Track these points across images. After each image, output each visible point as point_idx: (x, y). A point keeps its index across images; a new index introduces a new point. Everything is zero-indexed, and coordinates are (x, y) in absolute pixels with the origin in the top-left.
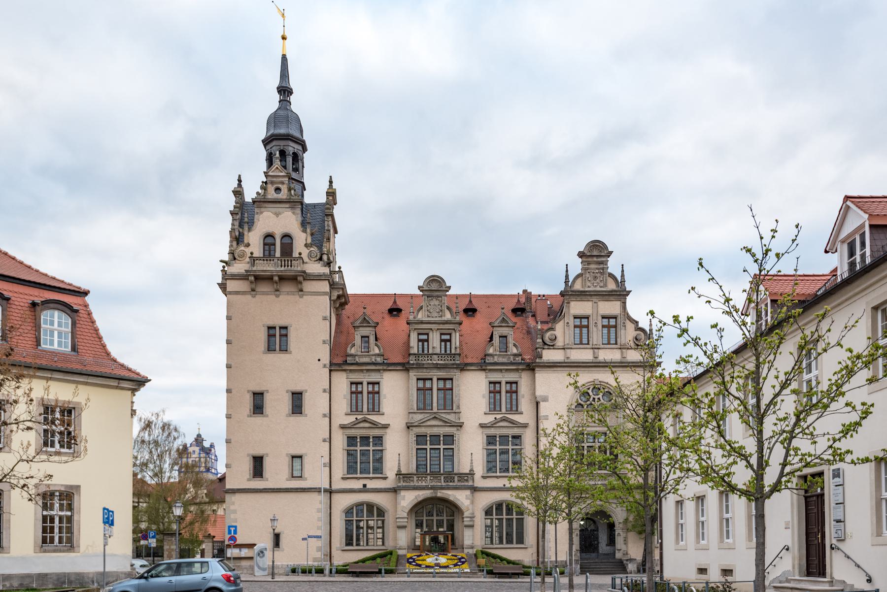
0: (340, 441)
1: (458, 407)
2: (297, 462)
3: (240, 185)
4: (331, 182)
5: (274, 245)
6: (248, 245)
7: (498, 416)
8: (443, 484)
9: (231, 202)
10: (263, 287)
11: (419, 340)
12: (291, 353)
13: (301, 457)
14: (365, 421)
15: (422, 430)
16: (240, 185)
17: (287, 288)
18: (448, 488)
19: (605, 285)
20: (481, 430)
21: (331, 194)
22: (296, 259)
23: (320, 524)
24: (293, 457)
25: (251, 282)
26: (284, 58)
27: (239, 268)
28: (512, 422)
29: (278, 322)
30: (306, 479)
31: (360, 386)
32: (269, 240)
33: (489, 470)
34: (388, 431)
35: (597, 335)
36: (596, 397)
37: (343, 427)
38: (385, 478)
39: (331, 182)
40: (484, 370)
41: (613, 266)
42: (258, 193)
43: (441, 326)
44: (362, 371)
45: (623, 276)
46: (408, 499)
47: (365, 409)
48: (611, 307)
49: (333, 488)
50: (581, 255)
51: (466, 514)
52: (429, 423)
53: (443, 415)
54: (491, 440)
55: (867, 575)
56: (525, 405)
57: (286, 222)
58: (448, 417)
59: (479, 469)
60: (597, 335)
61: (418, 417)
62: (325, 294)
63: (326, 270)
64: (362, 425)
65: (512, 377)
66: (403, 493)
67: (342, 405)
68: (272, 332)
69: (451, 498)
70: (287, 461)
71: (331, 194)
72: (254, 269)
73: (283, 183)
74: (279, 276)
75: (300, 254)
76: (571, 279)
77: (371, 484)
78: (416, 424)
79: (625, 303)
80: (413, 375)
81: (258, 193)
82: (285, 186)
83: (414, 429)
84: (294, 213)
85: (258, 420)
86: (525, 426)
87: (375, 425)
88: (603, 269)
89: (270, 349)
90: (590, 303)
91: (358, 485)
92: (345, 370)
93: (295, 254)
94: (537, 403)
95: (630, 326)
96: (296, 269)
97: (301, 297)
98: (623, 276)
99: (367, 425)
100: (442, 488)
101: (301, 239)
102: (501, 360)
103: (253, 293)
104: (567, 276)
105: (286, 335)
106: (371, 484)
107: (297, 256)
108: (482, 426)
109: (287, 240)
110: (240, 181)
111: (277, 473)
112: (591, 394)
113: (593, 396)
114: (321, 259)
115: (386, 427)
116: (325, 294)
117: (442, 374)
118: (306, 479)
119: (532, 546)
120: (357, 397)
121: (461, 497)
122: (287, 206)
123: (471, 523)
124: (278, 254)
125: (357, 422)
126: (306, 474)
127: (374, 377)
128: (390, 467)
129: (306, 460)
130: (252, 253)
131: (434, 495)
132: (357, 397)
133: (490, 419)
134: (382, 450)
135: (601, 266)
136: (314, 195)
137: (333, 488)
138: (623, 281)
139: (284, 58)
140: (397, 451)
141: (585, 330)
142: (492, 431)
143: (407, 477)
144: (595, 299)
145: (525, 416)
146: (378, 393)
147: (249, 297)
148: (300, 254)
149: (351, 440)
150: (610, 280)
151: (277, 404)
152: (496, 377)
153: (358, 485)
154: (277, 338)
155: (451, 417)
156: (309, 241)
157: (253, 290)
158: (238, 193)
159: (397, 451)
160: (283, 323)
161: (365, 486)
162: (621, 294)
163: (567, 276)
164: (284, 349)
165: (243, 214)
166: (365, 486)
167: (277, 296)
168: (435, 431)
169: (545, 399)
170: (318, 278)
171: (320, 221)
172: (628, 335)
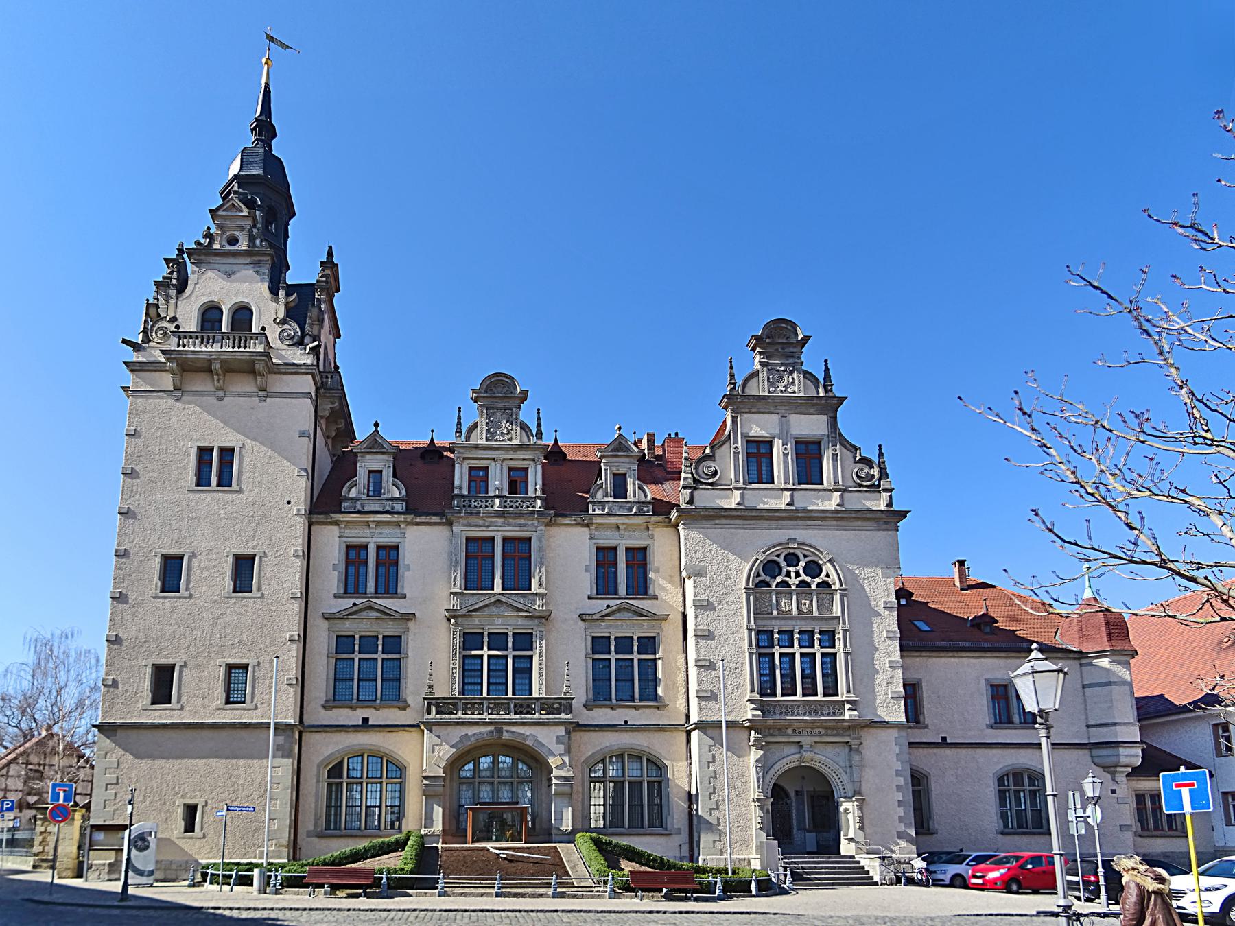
10: (201, 384)
14: (370, 608)
17: (245, 384)
21: (329, 265)
22: (255, 337)
23: (901, 781)
33: (595, 698)
34: (411, 624)
36: (792, 569)
37: (328, 617)
40: (587, 526)
42: (198, 243)
44: (367, 523)
47: (371, 587)
49: (307, 722)
57: (249, 288)
59: (580, 696)
64: (363, 615)
67: (330, 580)
71: (329, 265)
73: (242, 228)
74: (223, 362)
75: (264, 329)
77: (375, 717)
82: (246, 233)
84: (257, 272)
85: (170, 601)
88: (793, 365)
89: (202, 480)
90: (775, 418)
91: (355, 716)
92: (337, 523)
96: (252, 349)
97: (263, 399)
99: (375, 614)
103: (178, 393)
106: (375, 717)
111: (200, 700)
115: (408, 617)
116: (309, 395)
119: (679, 832)
120: (357, 572)
122: (248, 260)
132: (357, 572)
135: (791, 361)
136: (303, 269)
142: (602, 630)
143: (442, 705)
144: (782, 410)
147: (170, 402)
149: (343, 644)
151: (209, 576)
153: (355, 716)
154: (215, 467)
156: (281, 314)
159: (433, 661)
161: (365, 720)
166: (365, 720)
167: (220, 398)
168: (497, 626)
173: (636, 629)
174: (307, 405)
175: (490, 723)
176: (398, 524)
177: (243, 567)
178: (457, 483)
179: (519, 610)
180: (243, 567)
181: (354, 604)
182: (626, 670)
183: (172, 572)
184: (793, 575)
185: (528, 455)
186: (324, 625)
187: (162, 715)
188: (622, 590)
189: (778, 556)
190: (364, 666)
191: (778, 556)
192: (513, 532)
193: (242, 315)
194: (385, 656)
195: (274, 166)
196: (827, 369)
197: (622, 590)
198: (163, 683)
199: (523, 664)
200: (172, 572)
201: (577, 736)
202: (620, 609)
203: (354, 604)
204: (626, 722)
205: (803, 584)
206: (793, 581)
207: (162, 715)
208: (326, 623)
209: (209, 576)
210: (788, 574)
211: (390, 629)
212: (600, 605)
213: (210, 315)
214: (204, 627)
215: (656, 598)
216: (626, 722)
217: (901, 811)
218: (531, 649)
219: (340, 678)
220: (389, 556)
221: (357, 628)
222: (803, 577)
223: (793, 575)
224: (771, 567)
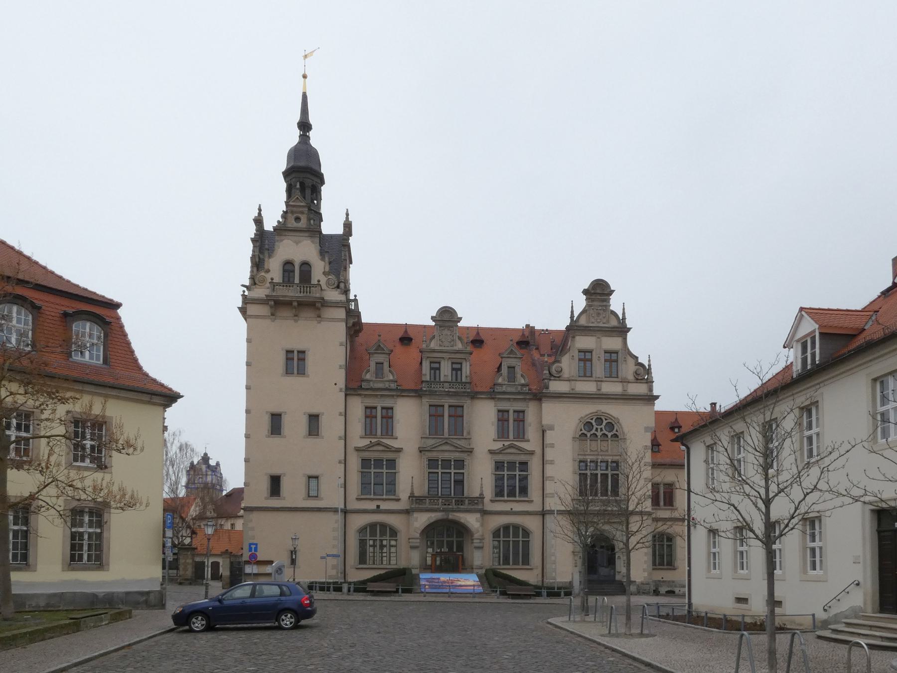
0: (354, 462)
1: (469, 433)
3: (260, 214)
4: (347, 215)
5: (293, 271)
6: (268, 271)
7: (506, 443)
9: (252, 230)
10: (286, 312)
11: (431, 369)
12: (308, 376)
14: (378, 444)
15: (433, 455)
16: (260, 214)
17: (308, 313)
18: (459, 511)
19: (608, 322)
20: (489, 456)
21: (348, 226)
25: (271, 307)
26: (305, 97)
27: (260, 293)
28: (519, 449)
29: (296, 346)
31: (374, 411)
32: (288, 267)
34: (401, 454)
35: (599, 368)
36: (599, 427)
37: (358, 450)
38: (398, 500)
39: (347, 215)
40: (493, 398)
41: (615, 304)
42: (279, 222)
43: (453, 356)
45: (624, 314)
46: (422, 520)
48: (613, 343)
50: (585, 292)
51: (476, 536)
53: (455, 441)
54: (499, 466)
56: (532, 432)
58: (459, 442)
59: (489, 493)
60: (599, 368)
61: (431, 442)
62: (340, 320)
63: (342, 298)
64: (375, 448)
65: (519, 406)
66: (416, 515)
67: (357, 428)
68: (290, 356)
69: (462, 521)
70: (304, 480)
71: (348, 226)
72: (274, 294)
73: (302, 213)
75: (319, 281)
76: (576, 315)
77: (384, 506)
79: (625, 339)
80: (426, 401)
81: (279, 222)
82: (305, 216)
86: (532, 453)
87: (389, 449)
89: (288, 372)
91: (372, 506)
93: (314, 281)
94: (543, 432)
95: (631, 362)
97: (319, 322)
98: (624, 314)
99: (381, 448)
100: (453, 511)
101: (319, 269)
102: (509, 389)
104: (572, 312)
105: (304, 359)
106: (384, 506)
107: (316, 283)
108: (491, 452)
109: (305, 268)
110: (260, 210)
112: (594, 424)
113: (595, 426)
114: (338, 287)
115: (399, 450)
116: (340, 320)
117: (453, 401)
121: (472, 520)
123: (481, 545)
124: (297, 281)
125: (372, 445)
126: (323, 494)
127: (388, 403)
128: (404, 489)
130: (272, 279)
131: (445, 517)
133: (498, 446)
135: (605, 304)
136: (331, 226)
137: (349, 507)
138: (624, 318)
139: (305, 97)
140: (410, 474)
141: (588, 364)
145: (532, 443)
146: (392, 417)
148: (319, 281)
149: (365, 463)
150: (613, 317)
151: (294, 425)
152: (504, 406)
153: (372, 506)
155: (462, 443)
156: (327, 269)
157: (272, 315)
158: (259, 221)
159: (410, 474)
160: (301, 348)
161: (378, 507)
162: (622, 330)
163: (572, 312)
164: (302, 372)
165: (263, 242)
166: (378, 507)
168: (446, 456)
169: (551, 428)
170: (336, 305)
171: (338, 251)
172: (628, 369)
174: (343, 326)
175: (443, 511)
176: (393, 396)
177: (314, 419)
178: (424, 372)
180: (314, 419)
182: (513, 479)
183: (276, 423)
185: (462, 356)
186: (355, 453)
187: (275, 503)
188: (511, 437)
190: (377, 469)
192: (453, 401)
193: (306, 266)
195: (313, 155)
196: (649, 361)
197: (511, 437)
198: (275, 484)
199: (459, 478)
200: (276, 423)
201: (487, 517)
202: (510, 447)
205: (604, 434)
206: (599, 434)
207: (275, 503)
209: (294, 425)
210: (597, 430)
213: (288, 266)
214: (295, 455)
217: (646, 558)
218: (463, 468)
219: (365, 486)
220: (388, 415)
222: (604, 431)
224: (588, 425)
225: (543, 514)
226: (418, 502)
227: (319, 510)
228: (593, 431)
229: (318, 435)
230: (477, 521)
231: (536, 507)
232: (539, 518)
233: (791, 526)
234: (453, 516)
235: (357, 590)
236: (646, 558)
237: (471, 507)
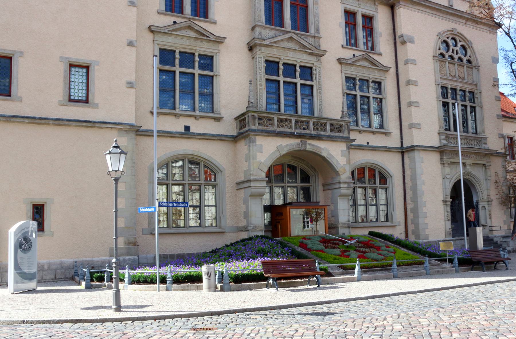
1: (317, 30)
2: (79, 93)
8: (313, 132)
13: (71, 100)
14: (190, 28)
18: (319, 138)
24: (71, 66)
30: (96, 106)
34: (221, 47)
38: (218, 119)
46: (268, 150)
52: (283, 44)
55: (116, 184)
64: (184, 33)
69: (324, 154)
70: (63, 68)
77: (197, 127)
78: (267, 42)
83: (263, 49)
87: (203, 35)
100: (312, 137)
106: (198, 127)
108: (340, 61)
115: (219, 41)
118: (96, 106)
126: (96, 96)
129: (95, 73)
131: (301, 148)
134: (212, 77)
140: (236, 82)
142: (352, 72)
159: (236, 82)
161: (187, 128)
166: (187, 128)
173: (300, 59)
179: (305, 47)
181: (175, 22)
184: (455, 52)
189: (448, 38)
191: (448, 38)
194: (202, 72)
203: (175, 22)
204: (130, 85)
206: (456, 56)
208: (151, 35)
211: (204, 48)
212: (167, 20)
215: (215, 23)
216: (368, 143)
221: (178, 43)
223: (455, 52)
225: (404, 151)
226: (245, 127)
227: (91, 124)
228: (450, 53)
229: (11, 58)
230: (342, 156)
231: (394, 142)
232: (398, 157)
233: (172, 205)
234: (312, 145)
235: (210, 277)
236: (425, 210)
237: (332, 134)
